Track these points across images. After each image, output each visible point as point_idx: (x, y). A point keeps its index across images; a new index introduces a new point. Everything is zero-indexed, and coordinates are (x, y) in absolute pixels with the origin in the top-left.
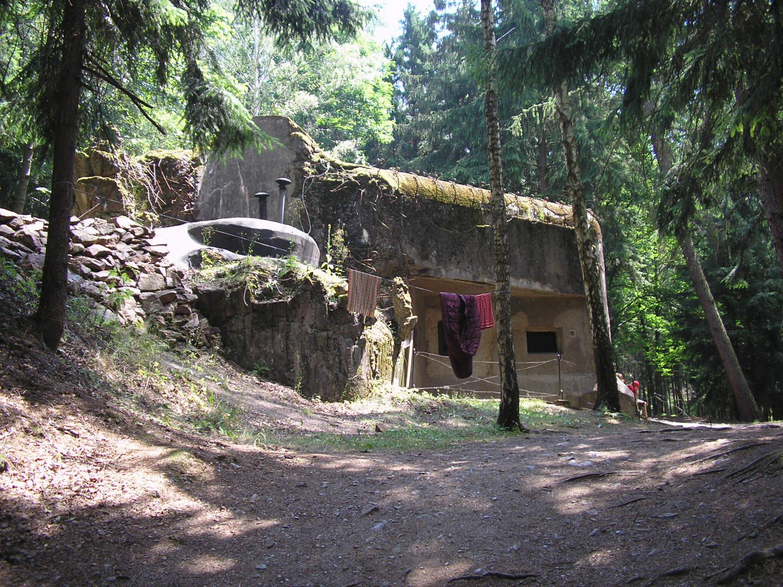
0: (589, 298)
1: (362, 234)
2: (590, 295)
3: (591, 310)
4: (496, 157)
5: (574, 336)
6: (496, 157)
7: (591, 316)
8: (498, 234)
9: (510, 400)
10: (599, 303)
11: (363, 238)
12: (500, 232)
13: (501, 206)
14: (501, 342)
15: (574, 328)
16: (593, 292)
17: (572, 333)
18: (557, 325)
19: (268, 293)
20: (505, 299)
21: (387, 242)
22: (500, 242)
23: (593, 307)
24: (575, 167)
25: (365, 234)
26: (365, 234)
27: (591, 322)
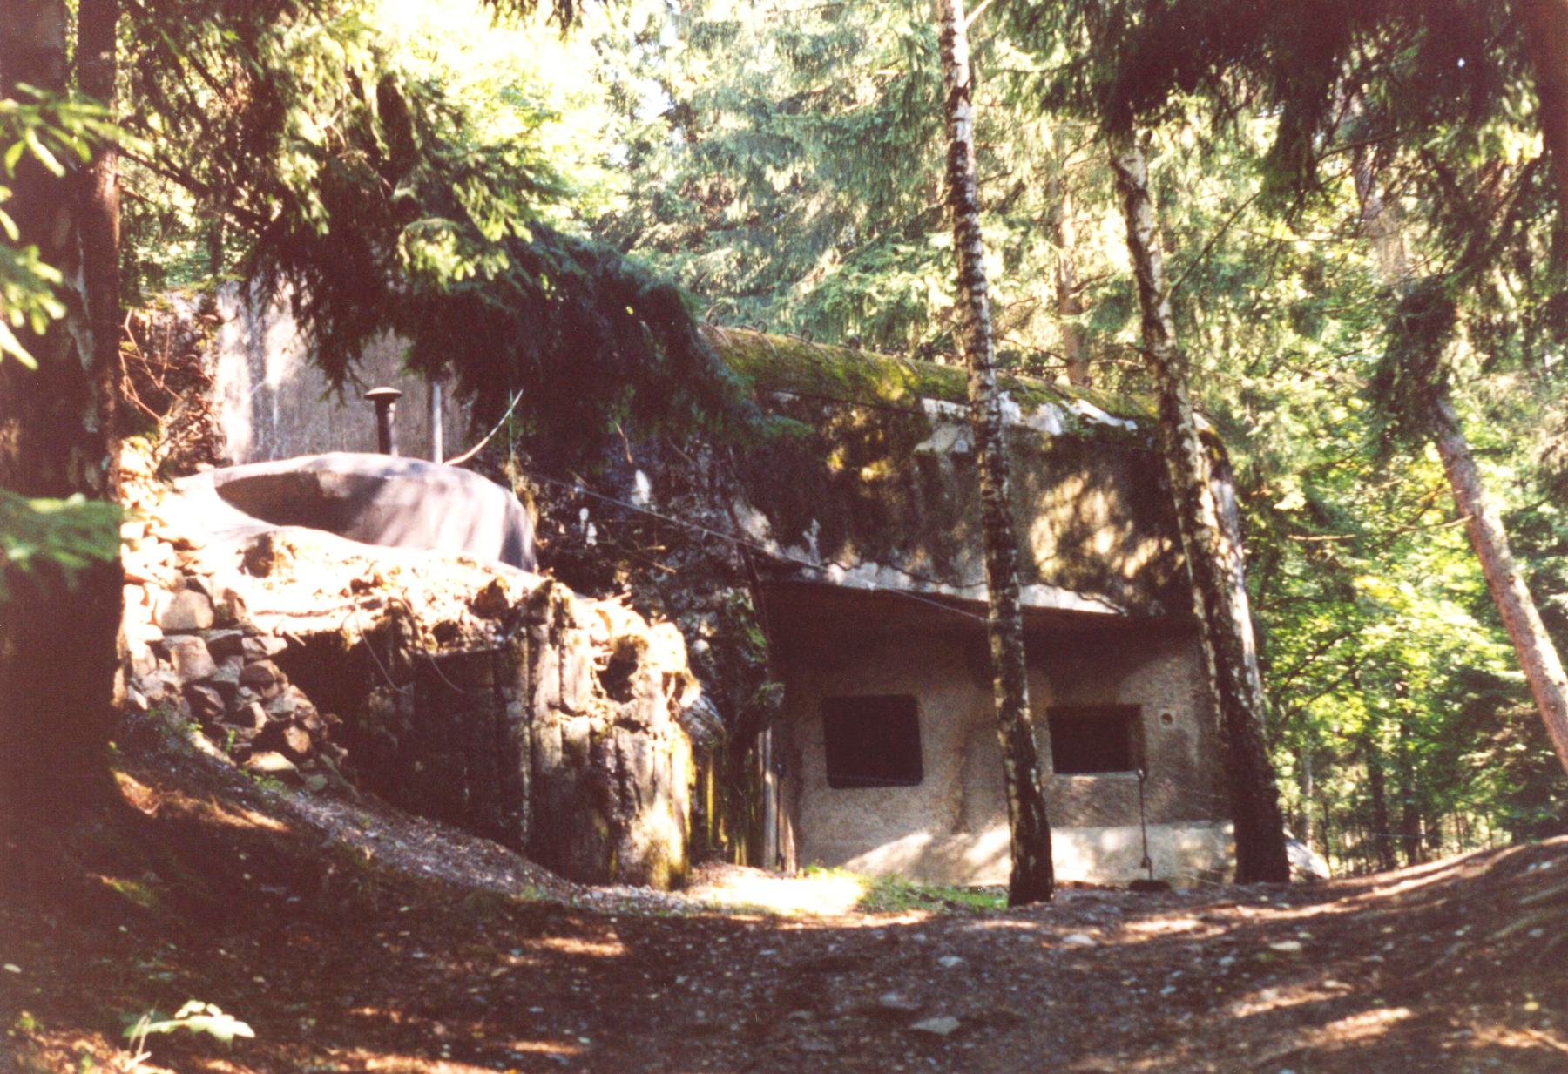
0: (1206, 625)
1: (632, 481)
2: (1209, 618)
3: (1212, 655)
4: (976, 299)
5: (1174, 726)
6: (976, 299)
7: (1213, 670)
8: (989, 478)
9: (1032, 861)
10: (1454, 887)
11: (637, 493)
12: (993, 473)
13: (992, 413)
14: (1008, 728)
15: (1168, 702)
16: (1216, 611)
17: (1167, 718)
18: (1125, 699)
19: (446, 632)
20: (1011, 629)
21: (698, 502)
22: (995, 496)
23: (1216, 647)
24: (1159, 304)
25: (642, 484)
26: (642, 484)
27: (1212, 684)
